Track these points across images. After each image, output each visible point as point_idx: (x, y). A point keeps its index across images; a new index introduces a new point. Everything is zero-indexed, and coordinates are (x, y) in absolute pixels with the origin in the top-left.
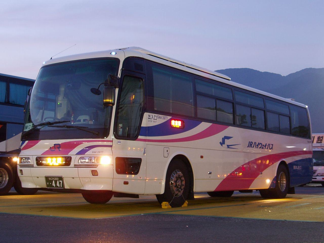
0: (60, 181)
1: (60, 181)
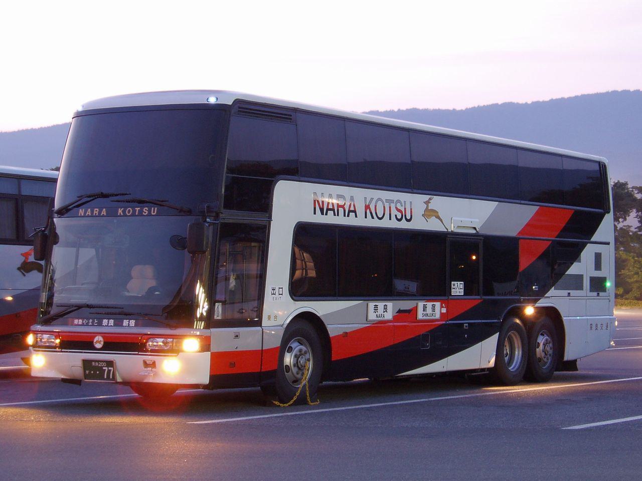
0: (110, 368)
1: (110, 368)
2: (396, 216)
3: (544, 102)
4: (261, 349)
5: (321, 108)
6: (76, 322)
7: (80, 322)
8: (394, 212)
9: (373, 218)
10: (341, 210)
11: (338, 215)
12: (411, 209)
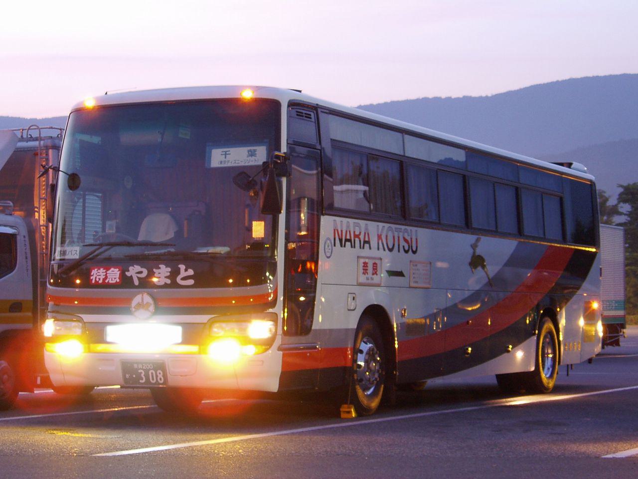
2: (404, 247)
3: (617, 76)
4: (38, 136)
5: (334, 104)
6: (37, 217)
7: (37, 214)
8: (403, 243)
9: (384, 250)
10: (357, 240)
11: (355, 247)
12: (416, 239)
